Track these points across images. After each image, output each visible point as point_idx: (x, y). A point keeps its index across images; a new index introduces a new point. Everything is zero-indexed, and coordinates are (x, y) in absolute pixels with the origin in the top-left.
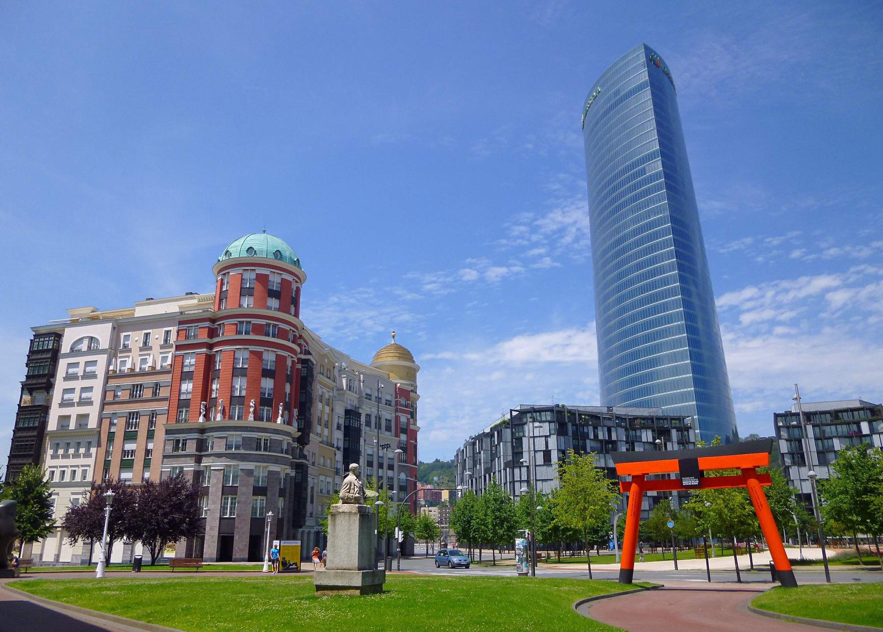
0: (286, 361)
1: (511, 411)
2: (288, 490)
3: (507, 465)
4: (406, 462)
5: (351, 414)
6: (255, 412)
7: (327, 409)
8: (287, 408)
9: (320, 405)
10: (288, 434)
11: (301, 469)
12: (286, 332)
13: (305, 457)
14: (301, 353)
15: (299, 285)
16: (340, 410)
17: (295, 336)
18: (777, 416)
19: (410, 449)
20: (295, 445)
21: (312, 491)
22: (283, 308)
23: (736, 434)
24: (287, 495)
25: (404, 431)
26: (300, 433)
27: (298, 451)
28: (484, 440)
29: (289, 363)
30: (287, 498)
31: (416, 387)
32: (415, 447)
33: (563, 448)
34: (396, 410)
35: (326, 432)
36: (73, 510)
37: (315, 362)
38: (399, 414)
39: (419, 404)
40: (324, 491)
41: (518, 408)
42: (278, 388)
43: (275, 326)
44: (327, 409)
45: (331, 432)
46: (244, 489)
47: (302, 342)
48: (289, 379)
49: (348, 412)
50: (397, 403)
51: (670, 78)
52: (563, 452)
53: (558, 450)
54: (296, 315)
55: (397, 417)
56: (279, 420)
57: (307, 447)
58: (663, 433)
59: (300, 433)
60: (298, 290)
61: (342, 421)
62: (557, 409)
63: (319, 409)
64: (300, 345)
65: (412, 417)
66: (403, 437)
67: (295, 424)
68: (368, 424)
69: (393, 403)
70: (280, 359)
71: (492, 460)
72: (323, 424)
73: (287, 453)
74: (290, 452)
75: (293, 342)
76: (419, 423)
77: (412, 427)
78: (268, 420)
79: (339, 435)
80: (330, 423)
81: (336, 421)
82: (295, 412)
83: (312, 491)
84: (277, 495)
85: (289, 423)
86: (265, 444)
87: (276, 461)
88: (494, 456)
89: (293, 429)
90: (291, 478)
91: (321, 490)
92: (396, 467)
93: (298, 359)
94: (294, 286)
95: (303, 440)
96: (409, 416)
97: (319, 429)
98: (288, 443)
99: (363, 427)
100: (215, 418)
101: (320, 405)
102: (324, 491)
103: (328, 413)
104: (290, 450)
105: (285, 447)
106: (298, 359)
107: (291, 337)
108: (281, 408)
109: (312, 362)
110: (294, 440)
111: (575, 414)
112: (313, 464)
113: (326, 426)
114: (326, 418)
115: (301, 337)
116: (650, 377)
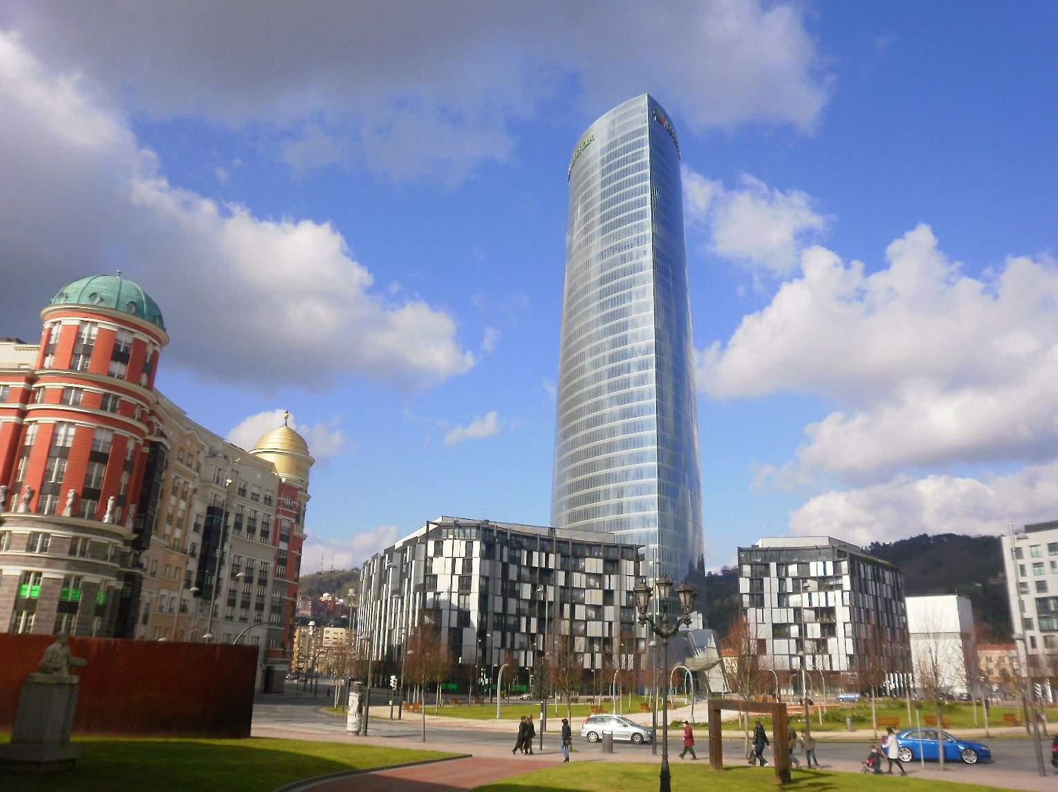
0: (126, 444)
1: (428, 523)
2: (108, 609)
3: (417, 588)
4: (283, 576)
5: (213, 512)
6: (73, 505)
7: (183, 505)
8: (119, 502)
9: (173, 500)
10: (117, 536)
11: (133, 582)
12: (133, 407)
13: (140, 566)
14: (151, 433)
15: (158, 349)
16: (200, 508)
17: (143, 413)
18: (740, 550)
19: (290, 561)
20: (128, 549)
21: (147, 609)
22: (133, 377)
23: (701, 565)
24: (107, 613)
25: (284, 538)
26: (135, 536)
27: (131, 557)
28: (395, 554)
29: (131, 446)
30: (107, 619)
31: (307, 484)
32: (299, 559)
33: (487, 574)
34: (278, 512)
35: (178, 534)
36: (161, 172)
37: (169, 447)
38: (280, 516)
39: (310, 506)
40: (166, 609)
41: (439, 520)
42: (113, 478)
43: (116, 398)
44: (183, 505)
45: (185, 535)
46: (46, 603)
47: (154, 420)
48: (127, 466)
49: (211, 510)
50: (279, 503)
51: (676, 143)
52: (487, 579)
53: (481, 576)
54: (149, 386)
55: (277, 520)
56: (107, 518)
57: (146, 553)
58: (612, 565)
59: (135, 536)
60: (155, 356)
61: (202, 522)
62: (485, 526)
63: (172, 504)
64: (149, 424)
65: (298, 521)
66: (283, 546)
67: (130, 525)
68: (238, 526)
69: (274, 503)
70: (119, 442)
71: (401, 582)
72: (175, 522)
73: (113, 560)
74: (118, 559)
75: (140, 420)
76: (306, 531)
77: (296, 533)
78: (91, 516)
79: (196, 539)
80: (184, 522)
81: (193, 520)
82: (132, 509)
83: (147, 609)
84: (93, 612)
85: (121, 522)
86: (84, 546)
87: (95, 569)
88: (403, 575)
89: (127, 530)
90: (116, 591)
91: (161, 608)
92: (270, 584)
93: (146, 441)
94: (150, 350)
95: (140, 544)
96: (294, 520)
97: (168, 529)
98: (117, 549)
99: (231, 530)
100: (16, 509)
101: (173, 500)
102: (166, 609)
103: (181, 511)
104: (122, 558)
105: (110, 552)
106: (146, 441)
107: (137, 413)
108: (110, 502)
109: (165, 447)
110: (126, 543)
111: (506, 534)
112: (153, 574)
113: (179, 525)
114: (179, 514)
115: (152, 413)
116: (594, 497)
